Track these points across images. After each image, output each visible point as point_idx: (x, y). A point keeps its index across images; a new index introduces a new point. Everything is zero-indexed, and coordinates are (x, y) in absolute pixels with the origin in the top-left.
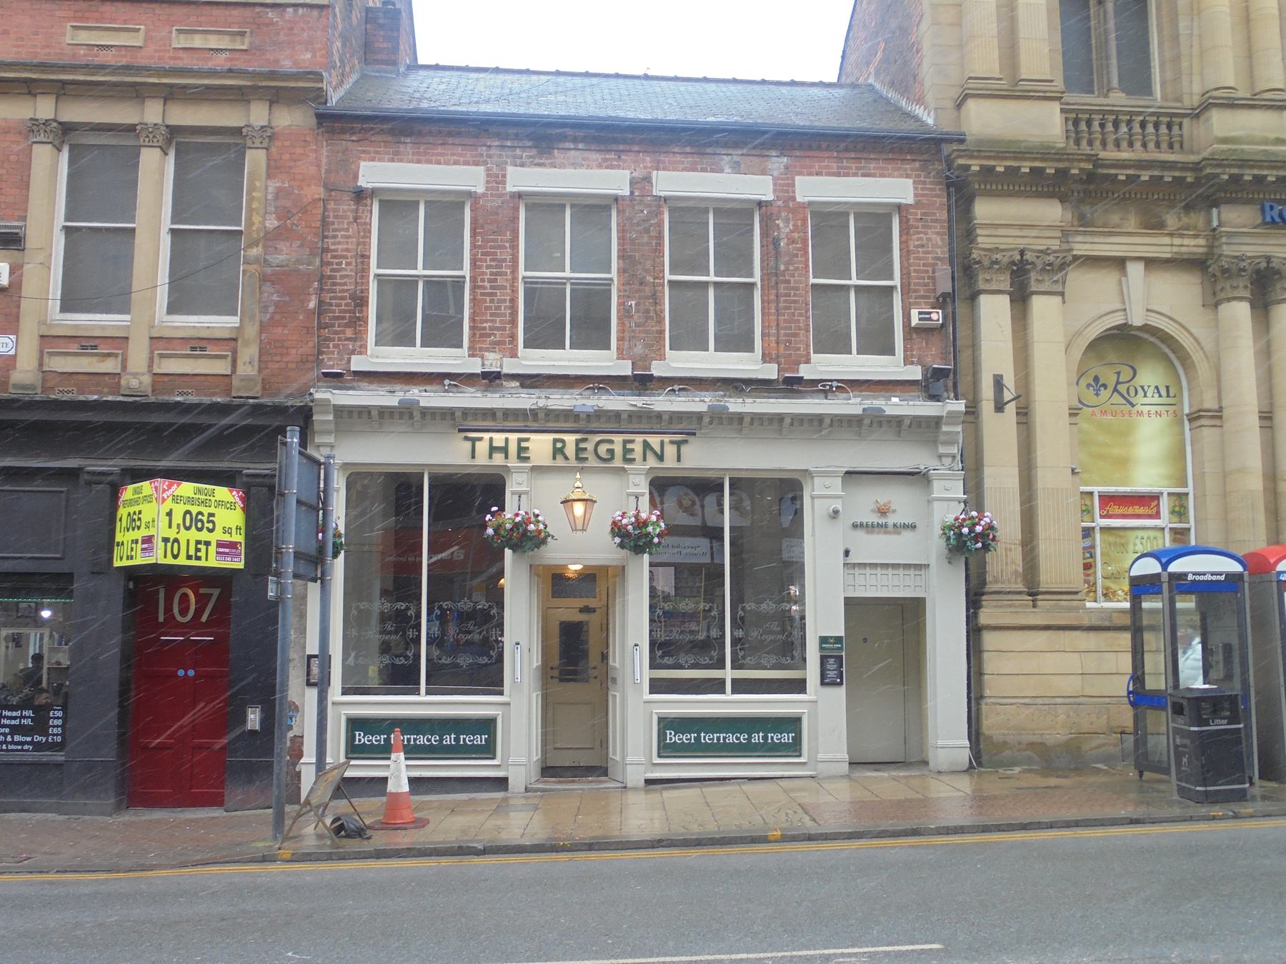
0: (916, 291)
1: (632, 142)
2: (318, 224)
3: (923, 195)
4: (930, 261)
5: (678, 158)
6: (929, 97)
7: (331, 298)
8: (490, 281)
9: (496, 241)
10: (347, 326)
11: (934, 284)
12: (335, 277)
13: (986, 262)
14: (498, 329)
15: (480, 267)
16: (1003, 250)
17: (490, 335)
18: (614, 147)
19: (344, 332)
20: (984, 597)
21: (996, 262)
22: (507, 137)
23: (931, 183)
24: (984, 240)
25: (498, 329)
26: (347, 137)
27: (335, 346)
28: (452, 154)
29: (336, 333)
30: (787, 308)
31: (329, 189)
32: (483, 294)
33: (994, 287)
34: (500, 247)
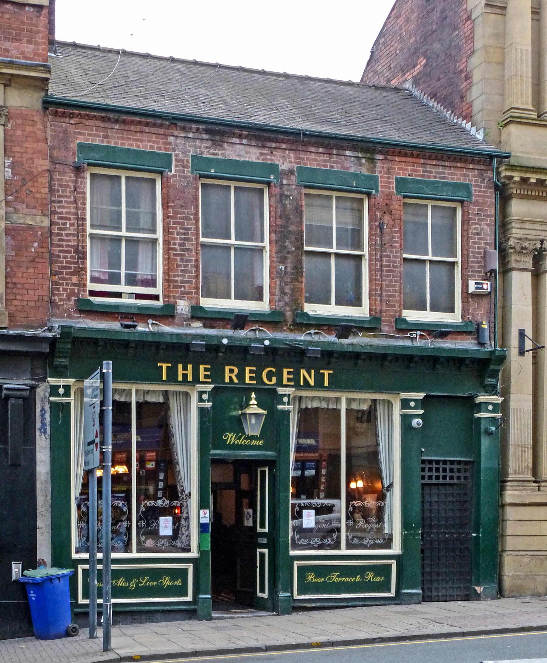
0: (472, 267)
1: (282, 141)
2: (47, 190)
3: (480, 196)
4: (482, 245)
5: (313, 156)
6: (478, 117)
7: (60, 251)
8: (180, 245)
9: (183, 213)
10: (72, 274)
11: (485, 262)
12: (62, 235)
13: (518, 248)
14: (187, 282)
15: (172, 233)
16: (530, 240)
17: (181, 287)
18: (269, 144)
19: (70, 279)
20: (508, 484)
21: (525, 249)
22: (190, 130)
23: (485, 187)
24: (516, 232)
25: (187, 282)
26: (67, 120)
27: (64, 290)
28: (149, 141)
29: (64, 279)
30: (388, 276)
31: (54, 161)
32: (175, 255)
33: (521, 266)
34: (186, 219)
